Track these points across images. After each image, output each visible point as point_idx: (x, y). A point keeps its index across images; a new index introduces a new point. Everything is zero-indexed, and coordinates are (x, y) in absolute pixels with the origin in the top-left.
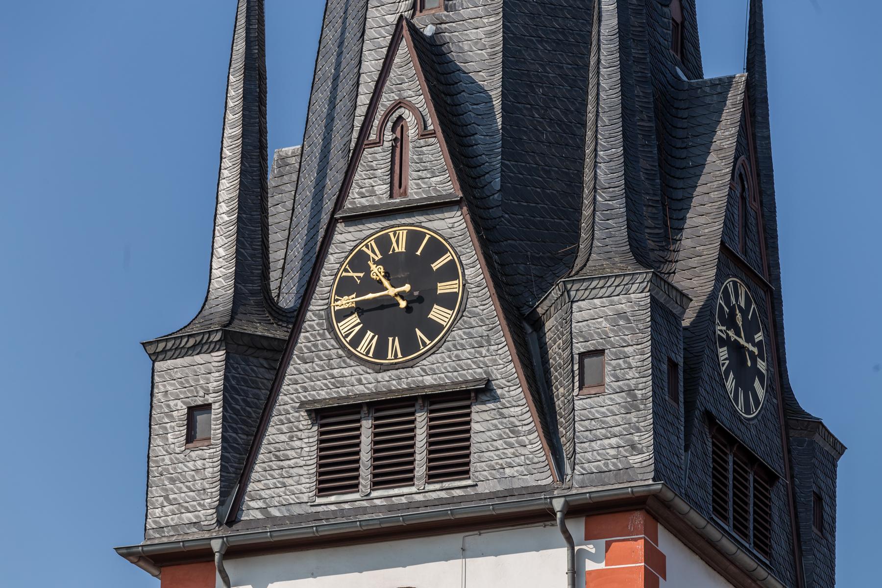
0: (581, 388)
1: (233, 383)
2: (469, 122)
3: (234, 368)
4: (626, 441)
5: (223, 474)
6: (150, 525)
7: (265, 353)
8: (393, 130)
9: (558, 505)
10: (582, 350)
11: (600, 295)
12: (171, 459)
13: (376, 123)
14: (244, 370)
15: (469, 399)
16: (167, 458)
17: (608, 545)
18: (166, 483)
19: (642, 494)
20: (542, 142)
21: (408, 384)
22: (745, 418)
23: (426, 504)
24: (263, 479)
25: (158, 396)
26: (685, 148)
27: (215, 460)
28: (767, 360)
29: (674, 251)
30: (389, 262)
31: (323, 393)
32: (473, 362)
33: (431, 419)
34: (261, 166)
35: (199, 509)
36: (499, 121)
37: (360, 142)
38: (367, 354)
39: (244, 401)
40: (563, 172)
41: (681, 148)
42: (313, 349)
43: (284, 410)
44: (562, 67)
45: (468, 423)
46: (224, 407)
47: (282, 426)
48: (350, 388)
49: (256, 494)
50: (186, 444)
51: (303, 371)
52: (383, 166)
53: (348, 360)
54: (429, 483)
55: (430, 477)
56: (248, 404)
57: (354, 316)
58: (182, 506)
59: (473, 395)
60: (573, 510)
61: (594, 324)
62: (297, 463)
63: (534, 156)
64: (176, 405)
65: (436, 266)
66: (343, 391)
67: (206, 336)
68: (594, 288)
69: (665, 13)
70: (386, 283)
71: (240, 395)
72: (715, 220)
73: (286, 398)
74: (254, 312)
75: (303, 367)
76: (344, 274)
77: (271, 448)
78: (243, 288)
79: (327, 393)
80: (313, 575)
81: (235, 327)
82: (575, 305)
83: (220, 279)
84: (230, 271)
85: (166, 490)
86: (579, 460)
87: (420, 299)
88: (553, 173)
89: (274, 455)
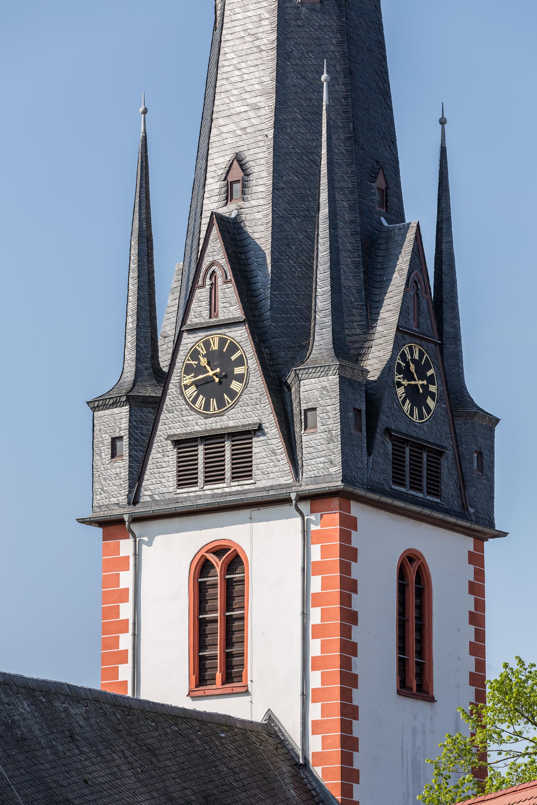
0: (305, 429)
1: (134, 423)
2: (254, 269)
3: (135, 415)
4: (328, 460)
5: (130, 476)
6: (95, 504)
7: (152, 405)
8: (211, 279)
9: (293, 496)
10: (306, 408)
11: (314, 377)
12: (104, 468)
13: (202, 274)
14: (140, 416)
15: (251, 433)
16: (102, 466)
17: (322, 516)
18: (102, 481)
19: (334, 490)
20: (295, 278)
21: (221, 425)
22: (418, 423)
23: (230, 494)
24: (150, 478)
25: (96, 432)
26: (383, 269)
27: (126, 468)
28: (437, 384)
29: (372, 334)
30: (210, 356)
31: (179, 430)
32: (253, 413)
33: (233, 445)
34: (149, 293)
35: (119, 496)
36: (270, 268)
37: (194, 286)
38: (200, 409)
39: (141, 433)
40: (306, 294)
41: (380, 269)
42: (173, 405)
43: (160, 440)
44: (307, 231)
45: (251, 448)
46: (129, 438)
47: (159, 449)
48: (192, 427)
49: (147, 487)
50: (112, 458)
51: (169, 418)
52: (205, 300)
53: (191, 412)
54: (232, 482)
55: (233, 478)
56: (143, 434)
57: (193, 386)
58: (110, 494)
59: (252, 432)
60: (302, 498)
61: (311, 393)
62: (167, 470)
63: (290, 287)
64: (105, 437)
65: (233, 358)
66: (189, 430)
67: (118, 398)
68: (310, 373)
69: (373, 187)
70: (208, 368)
71: (138, 430)
72: (394, 315)
73: (161, 433)
74: (147, 380)
75: (169, 415)
76: (188, 362)
77: (154, 461)
78: (140, 366)
79: (181, 430)
80: (177, 532)
81: (134, 393)
82: (301, 382)
83: (129, 361)
84: (133, 357)
85: (102, 485)
86: (305, 470)
87: (226, 376)
88: (301, 296)
89: (155, 465)
